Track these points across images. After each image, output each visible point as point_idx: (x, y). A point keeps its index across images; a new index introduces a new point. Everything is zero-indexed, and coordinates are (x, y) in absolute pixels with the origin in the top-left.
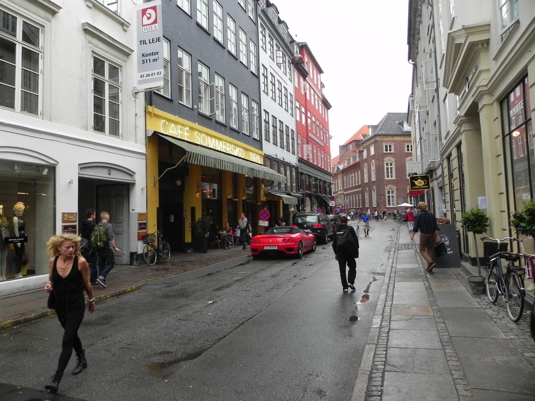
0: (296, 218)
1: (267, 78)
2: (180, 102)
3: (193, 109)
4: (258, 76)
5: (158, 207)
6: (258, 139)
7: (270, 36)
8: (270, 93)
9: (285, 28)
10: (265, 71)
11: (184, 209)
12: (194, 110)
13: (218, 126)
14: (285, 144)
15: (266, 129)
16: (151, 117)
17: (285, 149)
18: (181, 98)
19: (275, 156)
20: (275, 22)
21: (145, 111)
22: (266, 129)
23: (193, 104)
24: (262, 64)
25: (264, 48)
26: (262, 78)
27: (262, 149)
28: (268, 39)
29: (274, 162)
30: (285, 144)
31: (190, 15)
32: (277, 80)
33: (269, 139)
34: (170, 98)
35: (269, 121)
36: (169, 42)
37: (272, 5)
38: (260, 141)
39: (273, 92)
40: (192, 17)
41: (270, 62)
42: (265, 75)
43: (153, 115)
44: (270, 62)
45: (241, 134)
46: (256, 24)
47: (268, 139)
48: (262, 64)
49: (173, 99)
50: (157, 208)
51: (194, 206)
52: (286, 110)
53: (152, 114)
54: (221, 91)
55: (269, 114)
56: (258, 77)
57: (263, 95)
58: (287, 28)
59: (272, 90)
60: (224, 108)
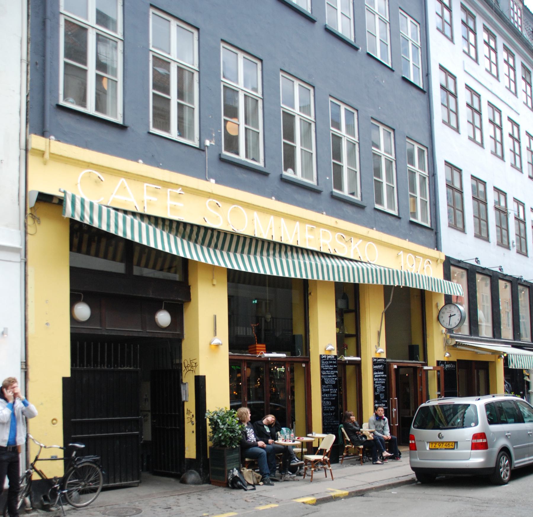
0: (276, 434)
1: (519, 142)
2: (378, 206)
3: (201, 149)
4: (425, 90)
5: (68, 374)
6: (428, 225)
7: (505, 48)
8: (508, 156)
10: (515, 128)
11: (184, 381)
12: (204, 151)
14: (513, 237)
15: (520, 233)
16: (45, 163)
17: (514, 250)
18: (379, 201)
19: (474, 263)
21: (26, 150)
22: (520, 233)
25: (448, 34)
27: (437, 246)
28: (503, 55)
30: (513, 237)
31: (391, 67)
33: (527, 251)
34: (397, 214)
35: (525, 219)
38: (432, 230)
39: (515, 154)
41: (464, 62)
42: (516, 136)
43: (50, 157)
44: (464, 62)
45: (368, 210)
47: (524, 251)
48: (526, 132)
49: (401, 216)
50: (65, 379)
51: (201, 374)
52: (517, 169)
53: (47, 156)
55: (487, 185)
60: (358, 170)
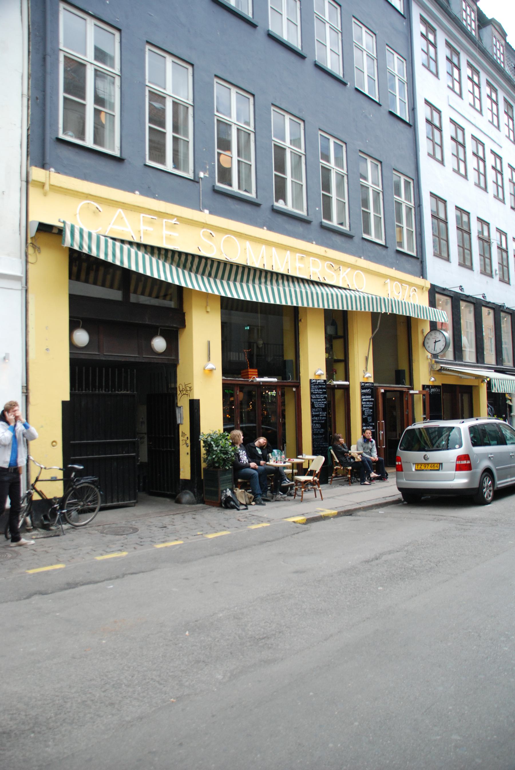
2: (365, 236)
3: (195, 181)
4: (411, 123)
5: (67, 398)
6: (414, 254)
8: (491, 187)
9: (496, 34)
10: (498, 161)
12: (198, 182)
13: (280, 219)
14: (496, 266)
15: (502, 262)
17: (496, 278)
18: (367, 230)
20: (472, 26)
21: (27, 182)
23: (196, 170)
24: (509, 164)
26: (422, 128)
27: (423, 274)
29: (502, 314)
30: (496, 266)
32: (507, 165)
33: (509, 279)
36: (302, 124)
37: (492, 22)
38: (418, 258)
40: (381, 103)
42: (499, 168)
46: (407, 17)
47: (506, 279)
49: (387, 246)
50: (64, 403)
51: (196, 397)
53: (47, 187)
54: (375, 184)
56: (412, 126)
57: (425, 162)
58: (504, 35)
59: (478, 171)
